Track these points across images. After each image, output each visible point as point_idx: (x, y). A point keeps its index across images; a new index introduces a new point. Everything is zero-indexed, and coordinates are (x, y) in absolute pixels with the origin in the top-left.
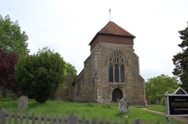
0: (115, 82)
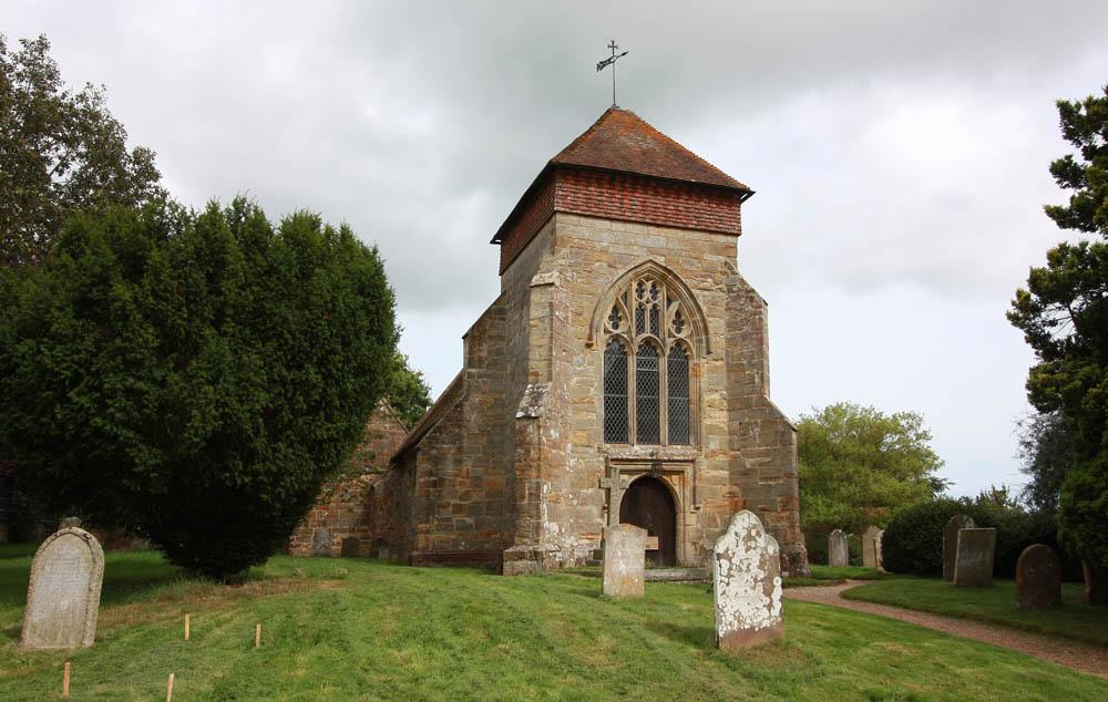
0: (640, 441)
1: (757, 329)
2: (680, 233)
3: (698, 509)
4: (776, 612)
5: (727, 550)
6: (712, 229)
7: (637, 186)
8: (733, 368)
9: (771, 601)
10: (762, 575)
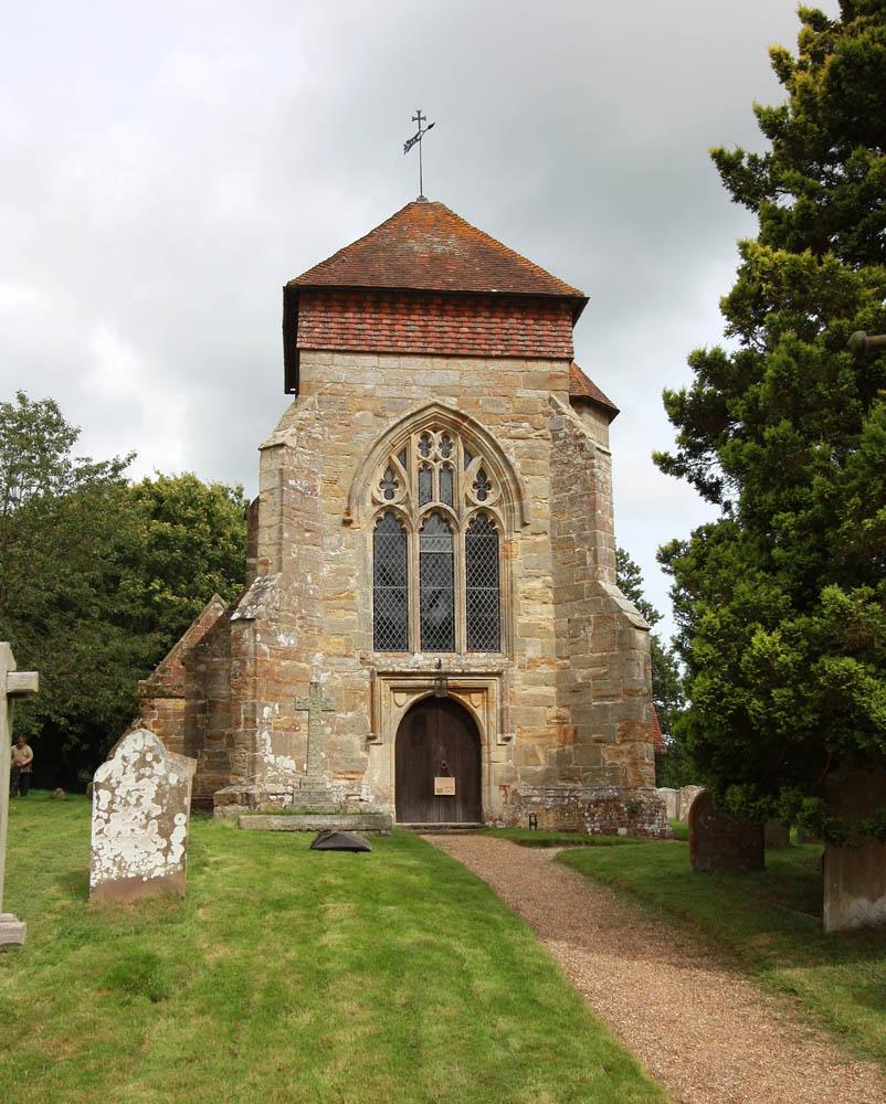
0: (425, 648)
1: (588, 489)
2: (480, 364)
3: (508, 739)
4: (175, 858)
5: (110, 778)
6: (527, 354)
7: (315, 303)
8: (561, 545)
9: (170, 844)
10: (157, 810)
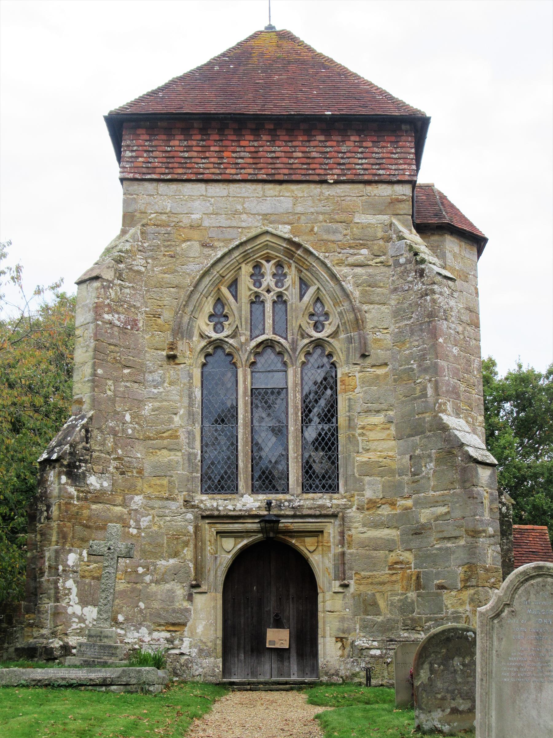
0: (255, 490)
2: (315, 189)
